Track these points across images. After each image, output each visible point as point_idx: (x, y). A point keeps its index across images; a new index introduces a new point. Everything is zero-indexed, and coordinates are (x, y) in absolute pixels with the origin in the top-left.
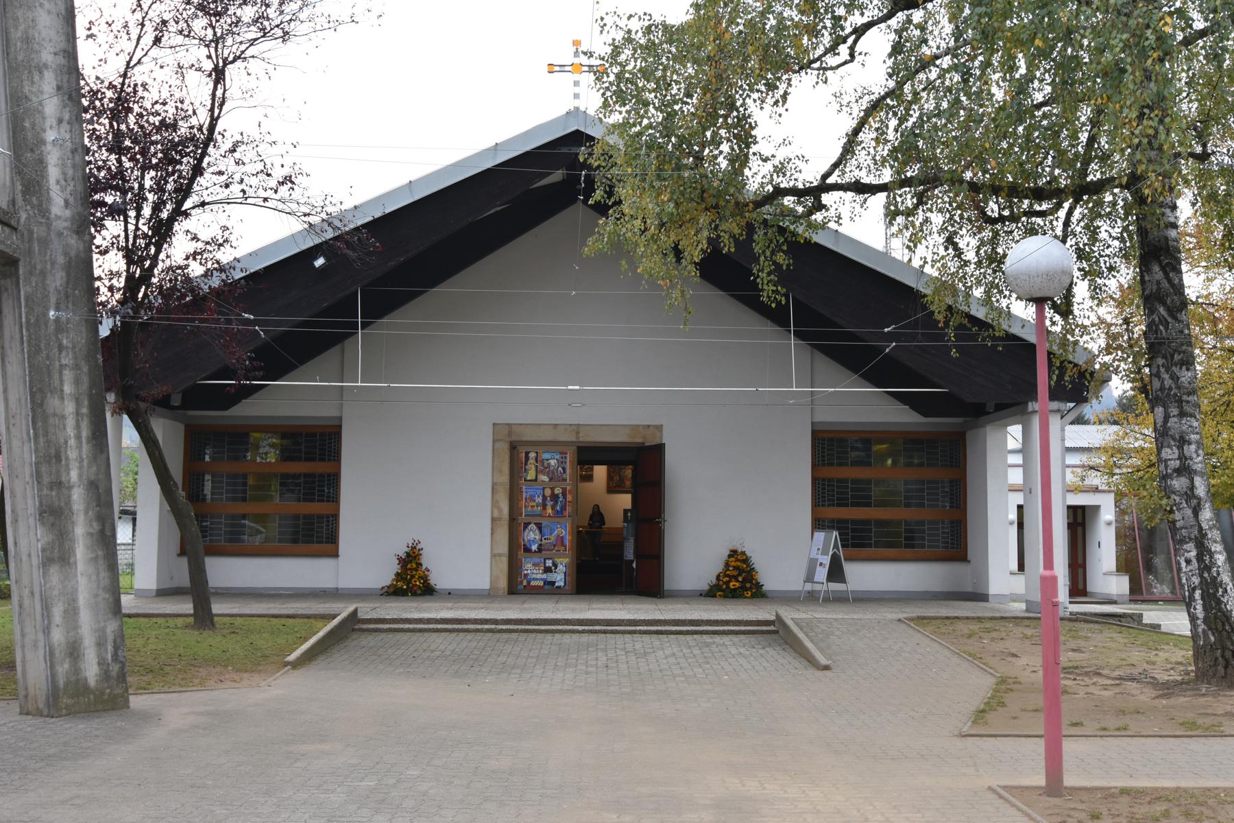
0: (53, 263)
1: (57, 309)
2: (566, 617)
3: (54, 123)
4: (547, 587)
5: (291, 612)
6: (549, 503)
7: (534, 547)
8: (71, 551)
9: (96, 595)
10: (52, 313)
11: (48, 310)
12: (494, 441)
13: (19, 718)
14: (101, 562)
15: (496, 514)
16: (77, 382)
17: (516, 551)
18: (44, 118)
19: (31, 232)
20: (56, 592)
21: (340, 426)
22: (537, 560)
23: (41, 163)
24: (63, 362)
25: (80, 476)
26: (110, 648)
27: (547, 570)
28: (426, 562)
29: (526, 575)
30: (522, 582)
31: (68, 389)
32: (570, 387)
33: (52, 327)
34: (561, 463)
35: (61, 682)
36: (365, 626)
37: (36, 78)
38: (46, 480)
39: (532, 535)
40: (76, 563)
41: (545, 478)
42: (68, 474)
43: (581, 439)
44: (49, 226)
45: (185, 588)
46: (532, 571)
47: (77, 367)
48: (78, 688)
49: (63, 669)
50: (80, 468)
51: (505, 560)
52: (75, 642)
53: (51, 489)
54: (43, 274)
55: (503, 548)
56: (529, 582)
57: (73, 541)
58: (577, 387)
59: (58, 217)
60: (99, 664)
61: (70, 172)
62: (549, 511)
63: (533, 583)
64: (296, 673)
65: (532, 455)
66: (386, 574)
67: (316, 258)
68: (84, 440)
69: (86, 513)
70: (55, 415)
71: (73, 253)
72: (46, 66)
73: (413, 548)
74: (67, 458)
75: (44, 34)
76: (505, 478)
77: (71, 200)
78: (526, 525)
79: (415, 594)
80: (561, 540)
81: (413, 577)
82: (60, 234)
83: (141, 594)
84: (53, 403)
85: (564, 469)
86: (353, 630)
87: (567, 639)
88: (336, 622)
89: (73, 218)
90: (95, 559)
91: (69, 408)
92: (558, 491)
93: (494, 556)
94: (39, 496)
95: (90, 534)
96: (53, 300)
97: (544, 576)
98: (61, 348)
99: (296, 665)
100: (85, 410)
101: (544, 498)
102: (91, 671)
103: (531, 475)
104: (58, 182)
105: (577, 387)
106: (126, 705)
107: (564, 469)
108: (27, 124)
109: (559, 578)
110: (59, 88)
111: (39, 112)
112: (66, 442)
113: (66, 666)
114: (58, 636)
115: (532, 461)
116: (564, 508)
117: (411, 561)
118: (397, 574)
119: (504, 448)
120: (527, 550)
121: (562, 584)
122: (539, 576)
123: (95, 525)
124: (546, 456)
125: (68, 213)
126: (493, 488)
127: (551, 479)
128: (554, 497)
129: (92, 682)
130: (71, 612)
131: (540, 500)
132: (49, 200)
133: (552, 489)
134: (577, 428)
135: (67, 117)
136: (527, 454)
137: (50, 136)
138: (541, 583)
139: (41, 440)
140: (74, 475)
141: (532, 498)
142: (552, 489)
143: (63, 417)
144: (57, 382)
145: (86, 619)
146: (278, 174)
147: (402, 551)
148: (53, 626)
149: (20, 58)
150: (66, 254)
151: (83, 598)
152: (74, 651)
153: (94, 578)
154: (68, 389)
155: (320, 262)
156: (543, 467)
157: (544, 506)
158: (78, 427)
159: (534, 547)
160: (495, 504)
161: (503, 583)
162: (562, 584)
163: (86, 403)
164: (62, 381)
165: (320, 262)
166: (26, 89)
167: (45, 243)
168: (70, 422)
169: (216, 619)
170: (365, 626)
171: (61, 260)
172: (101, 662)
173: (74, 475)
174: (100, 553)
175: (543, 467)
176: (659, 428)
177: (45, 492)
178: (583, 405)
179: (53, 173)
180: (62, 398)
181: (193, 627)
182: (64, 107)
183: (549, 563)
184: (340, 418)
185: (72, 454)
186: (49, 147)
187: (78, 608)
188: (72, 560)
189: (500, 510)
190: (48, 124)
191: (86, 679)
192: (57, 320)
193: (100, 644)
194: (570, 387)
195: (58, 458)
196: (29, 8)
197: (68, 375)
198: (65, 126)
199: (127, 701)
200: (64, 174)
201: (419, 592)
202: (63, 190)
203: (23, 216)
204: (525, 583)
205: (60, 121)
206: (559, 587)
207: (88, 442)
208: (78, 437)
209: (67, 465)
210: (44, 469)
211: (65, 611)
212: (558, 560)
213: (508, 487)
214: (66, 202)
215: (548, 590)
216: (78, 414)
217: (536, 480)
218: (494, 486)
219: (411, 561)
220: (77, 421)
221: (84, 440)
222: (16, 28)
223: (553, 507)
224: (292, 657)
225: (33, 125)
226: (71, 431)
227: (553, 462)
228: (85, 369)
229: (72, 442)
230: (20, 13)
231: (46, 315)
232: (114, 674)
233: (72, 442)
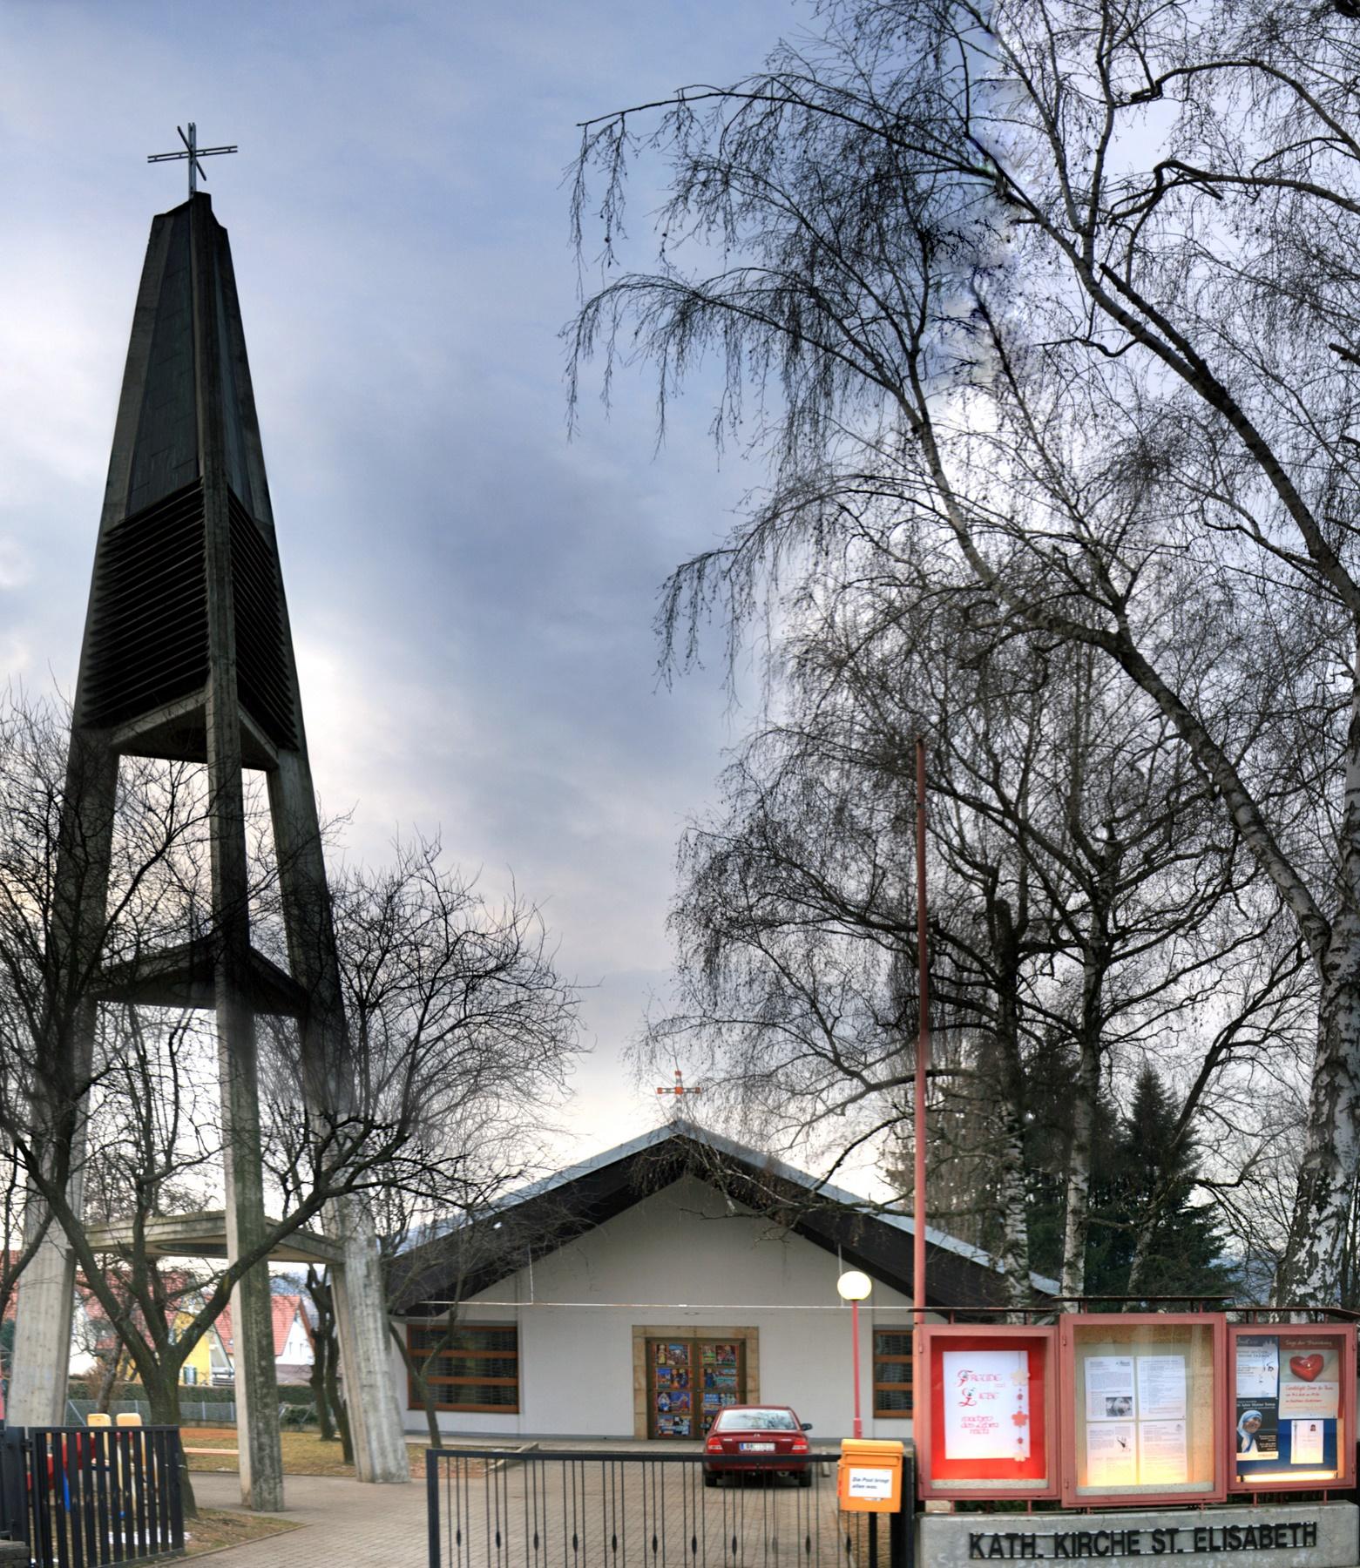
17: (653, 1412)
27: (676, 1424)
34: (685, 1353)
41: (672, 1363)
46: (665, 1424)
55: (643, 1408)
76: (642, 1362)
103: (662, 1360)
119: (641, 1342)
120: (661, 1410)
128: (679, 1375)
160: (636, 1379)
161: (644, 1432)
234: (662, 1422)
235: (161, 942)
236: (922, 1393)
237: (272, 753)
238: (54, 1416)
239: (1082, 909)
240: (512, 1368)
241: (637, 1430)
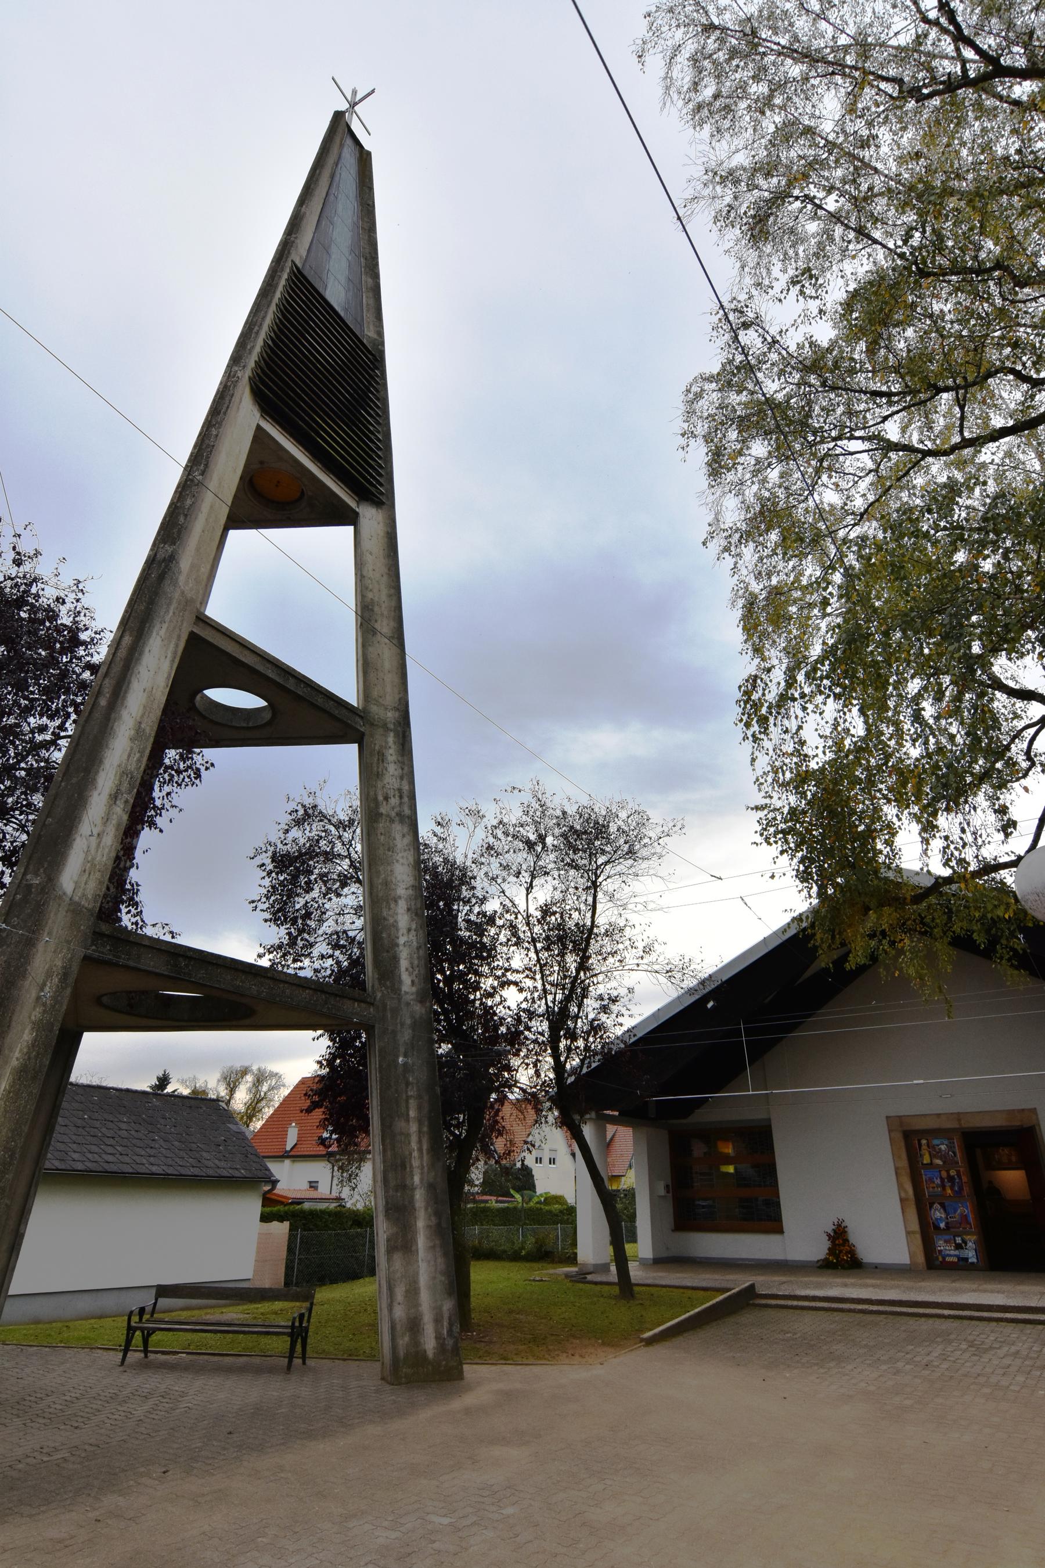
0: (402, 1024)
1: (405, 1056)
2: (946, 1300)
3: (405, 932)
4: (961, 1263)
5: (704, 1284)
6: (948, 1185)
7: (942, 1225)
8: (413, 1241)
9: (434, 1278)
10: (401, 1059)
11: (398, 1058)
12: (890, 1131)
13: (380, 1382)
14: (438, 1249)
15: (903, 1195)
16: (420, 1108)
17: (927, 1232)
18: (398, 930)
19: (385, 1006)
20: (398, 1275)
21: (770, 1126)
22: (947, 1237)
23: (395, 959)
24: (410, 1093)
25: (422, 1180)
26: (446, 1324)
27: (958, 1247)
28: (853, 1238)
29: (940, 1251)
30: (937, 1258)
31: (412, 1113)
32: (915, 1082)
33: (400, 1070)
34: (950, 1147)
35: (401, 1353)
36: (764, 1302)
37: (392, 906)
38: (392, 1183)
39: (938, 1214)
40: (417, 1251)
41: (939, 1162)
42: (412, 1178)
43: (964, 1125)
44: (399, 1000)
45: (278, 1290)
46: (944, 1247)
47: (419, 1097)
48: (417, 1358)
49: (404, 1341)
50: (422, 1174)
51: (918, 1236)
52: (416, 1318)
53: (397, 1191)
54: (394, 1033)
55: (915, 1226)
56: (944, 1258)
57: (415, 1233)
58: (921, 1081)
59: (406, 993)
60: (436, 1338)
61: (416, 962)
62: (949, 1191)
63: (948, 1259)
64: (651, 1349)
65: (924, 1142)
66: (817, 1249)
67: (708, 1002)
68: (425, 1152)
69: (426, 1209)
70: (402, 1134)
71: (417, 1016)
72: (400, 897)
73: (839, 1225)
74: (411, 1166)
75: (399, 878)
76: (904, 1163)
77: (416, 981)
78: (931, 1205)
79: (843, 1268)
80: (965, 1218)
81: (841, 1252)
82: (408, 1004)
83: (643, 1262)
84: (400, 1125)
85: (954, 1153)
86: (748, 1305)
87: (925, 1325)
88: (728, 1294)
89: (417, 993)
90: (433, 1247)
91: (414, 1128)
92: (953, 1173)
93: (908, 1233)
94: (386, 1197)
95: (429, 1227)
96: (402, 1050)
97: (957, 1252)
98: (407, 1084)
99: (650, 1342)
100: (425, 1129)
101: (942, 1179)
102: (429, 1344)
103: (926, 1159)
104: (407, 969)
105: (921, 1081)
106: (460, 1376)
107: (954, 1153)
108: (384, 935)
109: (971, 1255)
110: (409, 910)
111: (394, 926)
112: (411, 1154)
113: (407, 1339)
114: (399, 1312)
115: (924, 1147)
116: (961, 1189)
117: (839, 1236)
118: (829, 1249)
119: (898, 1136)
120: (937, 1227)
121: (975, 1260)
122: (952, 1252)
123: (433, 1218)
124: (936, 1142)
125: (414, 989)
126: (896, 1173)
127: (944, 1162)
128: (951, 1179)
129: (430, 1354)
130: (413, 1292)
131: (938, 1181)
132: (400, 982)
133: (948, 1172)
134: (958, 1116)
135: (414, 926)
136: (919, 1141)
137: (402, 940)
138: (955, 1259)
139: (389, 1153)
140: (417, 1179)
141: (931, 1180)
142: (948, 1172)
143: (408, 1135)
144: (403, 1109)
145: (425, 1298)
146: (640, 945)
147: (830, 1229)
148: (395, 1304)
149: (381, 894)
150: (412, 1017)
151: (423, 1279)
152: (414, 1325)
153: (432, 1263)
154: (412, 1113)
155: (710, 1005)
156: (935, 1153)
157: (944, 1187)
158: (420, 1142)
159: (942, 1225)
160: (900, 1186)
161: (921, 1259)
162: (975, 1260)
163: (426, 1123)
164: (408, 1109)
165: (710, 1005)
166: (385, 914)
167: (396, 1011)
168: (414, 1139)
169: (636, 1289)
170: (764, 1302)
171: (408, 1021)
172: (438, 1337)
173: (417, 1179)
174: (438, 1242)
175: (935, 1153)
176: (1034, 1111)
177: (391, 1192)
178: (952, 1096)
179: (404, 964)
180: (408, 1121)
181: (616, 1297)
182: (413, 920)
183: (959, 1240)
184: (769, 1120)
185: (416, 1163)
186: (401, 948)
187: (419, 1289)
188: (414, 1248)
189: (906, 1192)
190: (400, 933)
191: (425, 1351)
192: (405, 1064)
193: (437, 1320)
194: (915, 1082)
195: (403, 1166)
196: (389, 864)
197: (413, 1103)
198: (413, 933)
199: (461, 1372)
200: (412, 964)
201: (846, 1265)
202: (410, 974)
203: (379, 995)
204: (940, 1259)
205: (409, 930)
206: (973, 1263)
207: (428, 1153)
208: (420, 1150)
209: (411, 1171)
210: (390, 1175)
211: (407, 1291)
212: (967, 1238)
213: (908, 1170)
214: (413, 982)
215: (961, 1267)
216: (420, 1132)
217: (931, 1163)
218: (897, 1169)
219: (839, 1236)
220: (420, 1138)
221: (425, 1152)
222: (378, 877)
223: (952, 1188)
224: (647, 1335)
225: (389, 935)
226: (414, 1145)
227: (943, 1147)
228: (426, 1098)
229: (415, 1154)
230: (381, 868)
231: (396, 1061)
232: (449, 1347)
233: (415, 1154)
234: (941, 1245)
235: (975, 18)
236: (956, 1291)
237: (353, 504)
238: (261, 1261)
239: (585, 974)
240: (768, 1172)
241: (912, 1256)
